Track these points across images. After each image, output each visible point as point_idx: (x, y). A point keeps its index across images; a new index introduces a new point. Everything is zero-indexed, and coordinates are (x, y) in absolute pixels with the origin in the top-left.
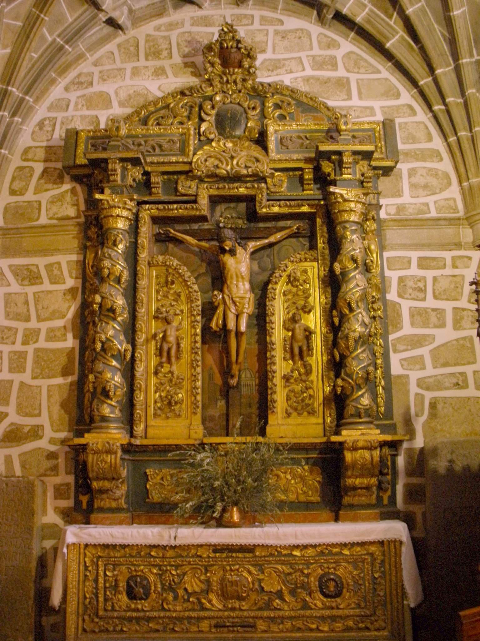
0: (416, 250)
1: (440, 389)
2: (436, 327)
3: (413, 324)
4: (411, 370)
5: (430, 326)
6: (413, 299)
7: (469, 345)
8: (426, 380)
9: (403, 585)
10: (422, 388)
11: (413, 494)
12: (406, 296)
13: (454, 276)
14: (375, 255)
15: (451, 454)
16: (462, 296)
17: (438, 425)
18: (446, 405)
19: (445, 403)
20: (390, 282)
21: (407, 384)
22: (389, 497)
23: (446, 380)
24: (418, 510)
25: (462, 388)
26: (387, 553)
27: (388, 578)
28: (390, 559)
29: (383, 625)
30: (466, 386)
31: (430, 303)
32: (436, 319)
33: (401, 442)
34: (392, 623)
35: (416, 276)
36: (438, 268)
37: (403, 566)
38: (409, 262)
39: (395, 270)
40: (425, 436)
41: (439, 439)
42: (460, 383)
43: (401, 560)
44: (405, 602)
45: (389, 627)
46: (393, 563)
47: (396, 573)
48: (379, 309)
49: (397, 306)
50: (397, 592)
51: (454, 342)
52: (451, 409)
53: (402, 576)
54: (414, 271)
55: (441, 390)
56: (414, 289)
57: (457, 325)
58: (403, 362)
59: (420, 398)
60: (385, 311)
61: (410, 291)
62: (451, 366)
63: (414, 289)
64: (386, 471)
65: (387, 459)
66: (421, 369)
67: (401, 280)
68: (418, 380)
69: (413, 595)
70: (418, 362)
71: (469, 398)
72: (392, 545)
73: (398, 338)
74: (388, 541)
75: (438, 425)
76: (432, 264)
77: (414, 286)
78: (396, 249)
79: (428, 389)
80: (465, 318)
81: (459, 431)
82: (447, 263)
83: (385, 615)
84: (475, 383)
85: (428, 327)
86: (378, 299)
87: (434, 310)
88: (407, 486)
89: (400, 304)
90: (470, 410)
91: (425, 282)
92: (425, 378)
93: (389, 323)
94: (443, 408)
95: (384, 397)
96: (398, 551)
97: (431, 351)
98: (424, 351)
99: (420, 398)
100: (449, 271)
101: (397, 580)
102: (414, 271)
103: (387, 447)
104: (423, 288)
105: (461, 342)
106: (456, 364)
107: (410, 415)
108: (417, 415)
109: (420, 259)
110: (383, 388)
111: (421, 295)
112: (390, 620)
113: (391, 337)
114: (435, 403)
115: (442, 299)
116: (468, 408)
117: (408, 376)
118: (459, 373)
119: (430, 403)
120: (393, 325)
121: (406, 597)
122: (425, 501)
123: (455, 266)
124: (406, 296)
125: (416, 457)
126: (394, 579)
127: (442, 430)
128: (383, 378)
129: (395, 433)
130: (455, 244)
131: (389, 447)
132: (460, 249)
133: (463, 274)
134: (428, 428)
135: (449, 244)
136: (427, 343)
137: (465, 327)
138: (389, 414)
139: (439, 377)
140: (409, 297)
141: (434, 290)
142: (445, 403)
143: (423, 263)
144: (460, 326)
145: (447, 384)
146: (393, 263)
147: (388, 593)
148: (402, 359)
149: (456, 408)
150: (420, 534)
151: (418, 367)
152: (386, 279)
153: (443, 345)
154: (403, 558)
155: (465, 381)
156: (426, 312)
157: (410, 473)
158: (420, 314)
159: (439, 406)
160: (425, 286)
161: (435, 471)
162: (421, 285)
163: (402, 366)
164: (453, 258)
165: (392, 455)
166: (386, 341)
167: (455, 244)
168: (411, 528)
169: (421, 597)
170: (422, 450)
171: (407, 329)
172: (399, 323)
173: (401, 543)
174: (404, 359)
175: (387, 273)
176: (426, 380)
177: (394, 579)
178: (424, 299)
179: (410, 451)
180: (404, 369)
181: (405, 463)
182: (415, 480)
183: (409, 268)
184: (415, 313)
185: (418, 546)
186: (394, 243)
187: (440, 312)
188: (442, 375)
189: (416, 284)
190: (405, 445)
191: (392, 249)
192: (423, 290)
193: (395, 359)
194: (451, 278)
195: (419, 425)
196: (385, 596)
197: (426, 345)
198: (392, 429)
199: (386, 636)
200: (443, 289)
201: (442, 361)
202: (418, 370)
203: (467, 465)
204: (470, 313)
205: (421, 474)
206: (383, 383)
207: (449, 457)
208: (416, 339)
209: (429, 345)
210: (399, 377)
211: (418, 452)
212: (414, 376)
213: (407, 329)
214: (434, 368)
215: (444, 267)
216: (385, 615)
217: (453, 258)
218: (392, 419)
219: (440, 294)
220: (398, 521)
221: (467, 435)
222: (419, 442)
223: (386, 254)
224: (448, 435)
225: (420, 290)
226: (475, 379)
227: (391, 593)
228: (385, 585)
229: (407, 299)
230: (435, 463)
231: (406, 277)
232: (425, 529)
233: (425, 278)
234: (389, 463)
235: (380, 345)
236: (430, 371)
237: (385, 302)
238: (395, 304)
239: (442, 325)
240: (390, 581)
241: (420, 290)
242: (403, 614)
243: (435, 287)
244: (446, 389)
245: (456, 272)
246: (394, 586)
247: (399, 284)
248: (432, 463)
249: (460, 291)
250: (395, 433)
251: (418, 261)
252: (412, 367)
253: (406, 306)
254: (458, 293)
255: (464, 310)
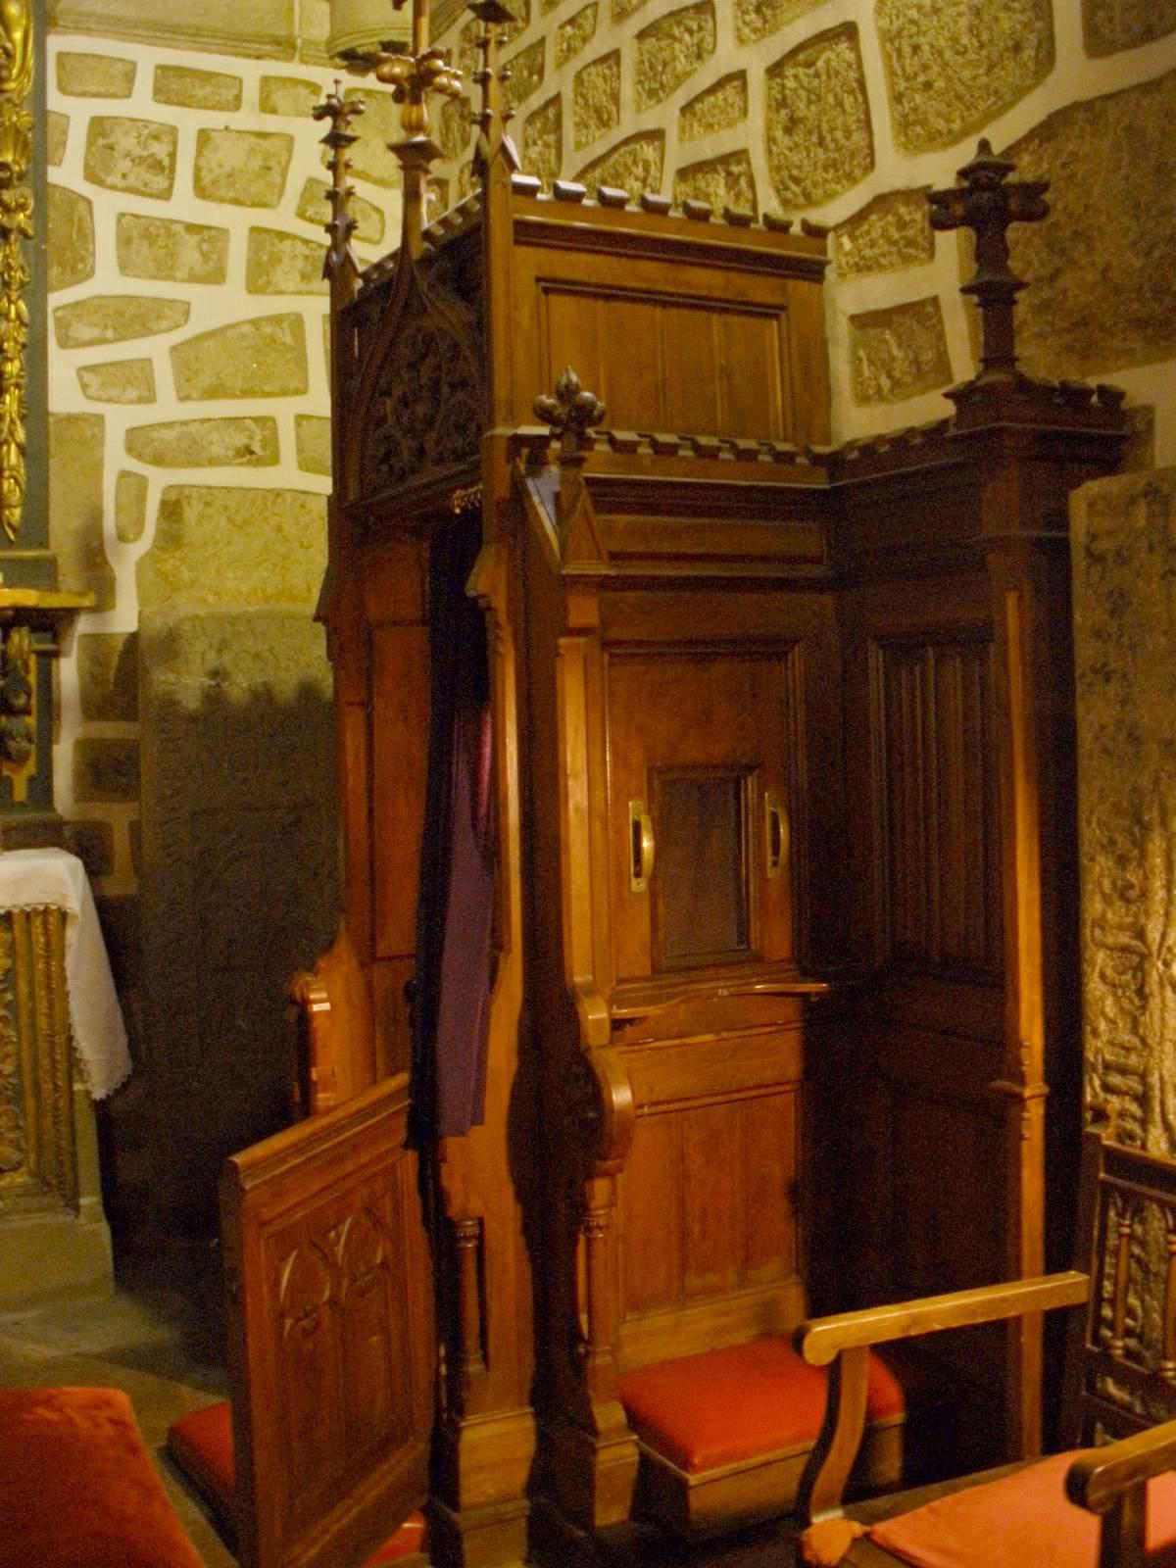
0: (151, 41)
1: (194, 463)
2: (193, 278)
3: (124, 267)
4: (109, 400)
5: (179, 275)
6: (128, 190)
7: (289, 340)
8: (155, 435)
9: (70, 1039)
10: (140, 457)
11: (105, 771)
12: (110, 180)
13: (263, 135)
14: (18, 35)
15: (219, 651)
16: (281, 195)
17: (184, 569)
18: (209, 511)
19: (207, 504)
20: (65, 133)
21: (98, 440)
22: (31, 780)
23: (215, 436)
24: (118, 816)
25: (260, 462)
26: (21, 950)
27: (24, 1020)
28: (31, 965)
29: (16, 1156)
30: (274, 459)
31: (184, 205)
32: (197, 256)
33: (70, 614)
34: (40, 1147)
35: (146, 123)
36: (218, 107)
37: (70, 986)
38: (130, 77)
39: (83, 94)
40: (143, 600)
41: (186, 606)
42: (256, 447)
43: (63, 970)
44: (77, 1087)
45: (32, 1158)
46: (40, 978)
47: (51, 1007)
48: (22, 207)
49: (81, 206)
50: (54, 1061)
51: (246, 329)
52: (223, 522)
53: (67, 1013)
54: (141, 104)
55: (198, 465)
56: (138, 161)
57: (259, 280)
58: (88, 377)
59: (133, 487)
60: (40, 215)
61: (125, 165)
62: (234, 396)
63: (138, 161)
64: (21, 701)
65: (26, 665)
66: (141, 400)
67: (99, 127)
68: (131, 431)
69: (99, 1055)
70: (136, 379)
71: (278, 494)
72: (38, 922)
73: (77, 304)
74: (22, 911)
75: (184, 569)
76: (200, 93)
77: (138, 151)
78: (89, 31)
79: (158, 460)
80: (286, 260)
81: (244, 588)
82: (246, 96)
83: (18, 1128)
84: (300, 451)
85: (174, 279)
86: (21, 177)
87: (192, 228)
88: (84, 746)
89: (89, 203)
90: (279, 529)
91: (175, 143)
92: (152, 427)
93: (52, 257)
94: (201, 517)
95: (23, 479)
96: (54, 940)
97: (174, 349)
98: (155, 349)
99: (133, 487)
100: (247, 118)
101: (51, 1026)
102: (141, 104)
103: (25, 630)
104: (166, 162)
105: (268, 329)
106: (247, 393)
107: (100, 535)
108: (122, 537)
109: (164, 71)
110: (22, 450)
111: (159, 182)
112: (33, 1140)
113: (55, 299)
114: (177, 503)
115: (222, 200)
116: (273, 521)
117: (99, 420)
118: (256, 420)
119: (164, 504)
120: (62, 264)
121: (81, 1072)
122: (139, 792)
123: (267, 107)
124: (110, 180)
125: (115, 661)
126: (43, 1023)
127: (193, 582)
128: (23, 418)
129: (54, 588)
130: (276, 41)
131: (34, 629)
132: (289, 58)
133: (290, 131)
134: (156, 578)
135: (258, 39)
136: (164, 324)
137: (283, 286)
138: (36, 529)
139: (193, 428)
140: (120, 183)
141: (198, 170)
142: (207, 504)
143: (172, 85)
144: (269, 283)
145: (216, 450)
146: (77, 73)
147: (26, 1067)
148: (86, 368)
149: (238, 519)
150: (119, 885)
151: (132, 393)
152: (51, 119)
153: (212, 334)
154: (69, 962)
155: (272, 442)
156: (170, 234)
157: (95, 707)
158: (148, 236)
159: (190, 514)
160: (173, 155)
161: (170, 703)
162: (160, 150)
163: (84, 387)
164: (266, 81)
165: (41, 654)
166: (38, 309)
167: (276, 41)
168: (96, 869)
169: (124, 1067)
170: (134, 638)
171: (107, 279)
172: (83, 259)
173: (63, 916)
174: (92, 369)
175: (56, 101)
176: (155, 435)
177: (43, 1023)
178: (166, 194)
179: (96, 643)
180: (89, 398)
181: (81, 677)
182: (110, 730)
183: (128, 96)
184: (136, 235)
185: (108, 911)
186: (84, 8)
187: (211, 238)
188: (203, 421)
189: (145, 147)
190: (83, 625)
191: (78, 28)
192: (165, 168)
193: (63, 368)
194: (253, 139)
195: (127, 565)
196: (18, 1071)
197: (161, 332)
198: (43, 573)
199: (22, 1185)
200: (227, 169)
201: (206, 380)
202: (132, 402)
203: (265, 684)
204: (300, 248)
205: (129, 714)
206: (21, 435)
207: (211, 657)
208: (132, 309)
209: (170, 330)
210: (71, 419)
211: (119, 645)
212: (119, 419)
213: (107, 279)
214: (181, 399)
215: (236, 104)
216: (18, 1128)
217: (266, 81)
218: (44, 544)
219: (213, 183)
220: (57, 849)
221: (267, 600)
222: (125, 618)
223: (55, 43)
224: (211, 599)
225: (157, 166)
226: (298, 438)
227: (36, 1065)
228: (19, 1043)
229: (114, 188)
230: (172, 677)
231: (116, 120)
232: (137, 869)
233: (173, 131)
234: (32, 679)
235: (19, 316)
236: (167, 407)
237: (42, 190)
238: (73, 199)
239: (216, 276)
240: (33, 1026)
241: (157, 166)
242: (72, 1124)
243: (203, 163)
244: (212, 462)
245: (271, 123)
246: (44, 1046)
247: (91, 141)
248: (161, 679)
249: (279, 180)
250: (54, 588)
251: (157, 79)
252: (114, 392)
253: (107, 208)
254: (271, 185)
255: (282, 236)
